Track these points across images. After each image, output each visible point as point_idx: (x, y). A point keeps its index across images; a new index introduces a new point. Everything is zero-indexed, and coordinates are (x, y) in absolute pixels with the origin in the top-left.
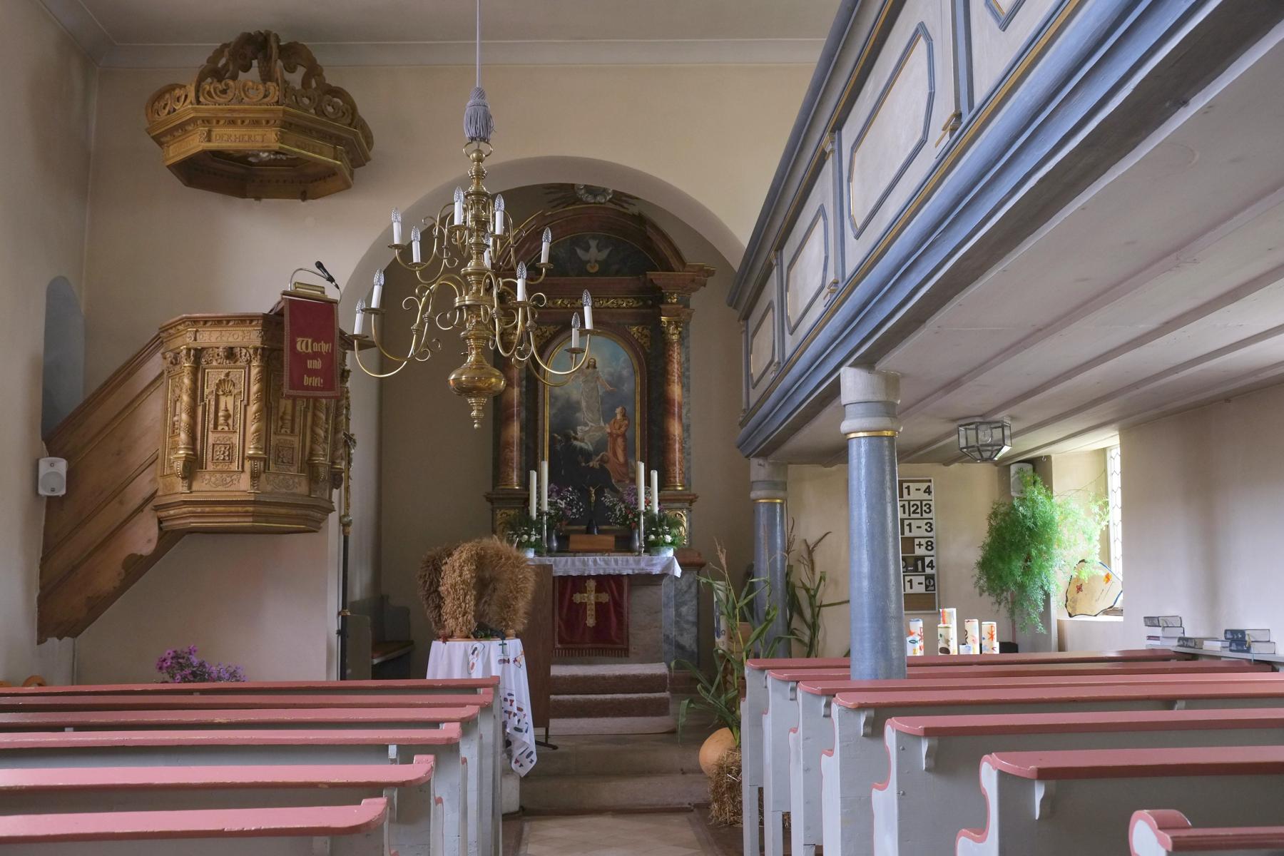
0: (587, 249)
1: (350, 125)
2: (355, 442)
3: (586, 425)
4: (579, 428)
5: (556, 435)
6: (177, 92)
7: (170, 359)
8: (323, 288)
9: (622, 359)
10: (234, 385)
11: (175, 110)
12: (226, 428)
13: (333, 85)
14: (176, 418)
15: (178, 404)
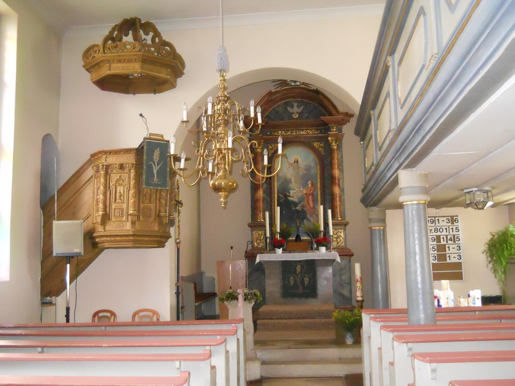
0: (292, 107)
1: (173, 59)
2: (182, 204)
3: (294, 190)
4: (291, 191)
5: (280, 195)
6: (95, 49)
7: (95, 170)
8: (163, 135)
9: (311, 158)
10: (123, 181)
11: (94, 57)
12: (120, 201)
13: (166, 41)
14: (98, 197)
15: (99, 190)
